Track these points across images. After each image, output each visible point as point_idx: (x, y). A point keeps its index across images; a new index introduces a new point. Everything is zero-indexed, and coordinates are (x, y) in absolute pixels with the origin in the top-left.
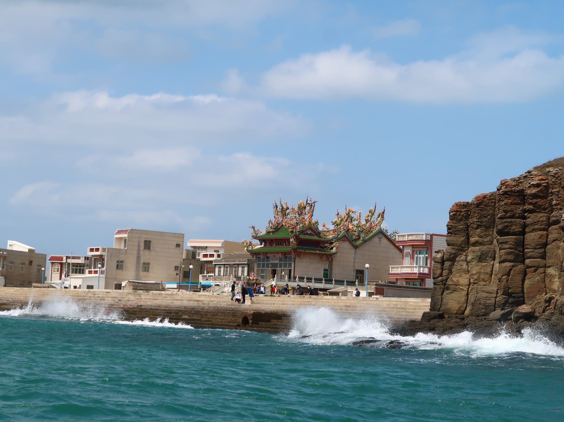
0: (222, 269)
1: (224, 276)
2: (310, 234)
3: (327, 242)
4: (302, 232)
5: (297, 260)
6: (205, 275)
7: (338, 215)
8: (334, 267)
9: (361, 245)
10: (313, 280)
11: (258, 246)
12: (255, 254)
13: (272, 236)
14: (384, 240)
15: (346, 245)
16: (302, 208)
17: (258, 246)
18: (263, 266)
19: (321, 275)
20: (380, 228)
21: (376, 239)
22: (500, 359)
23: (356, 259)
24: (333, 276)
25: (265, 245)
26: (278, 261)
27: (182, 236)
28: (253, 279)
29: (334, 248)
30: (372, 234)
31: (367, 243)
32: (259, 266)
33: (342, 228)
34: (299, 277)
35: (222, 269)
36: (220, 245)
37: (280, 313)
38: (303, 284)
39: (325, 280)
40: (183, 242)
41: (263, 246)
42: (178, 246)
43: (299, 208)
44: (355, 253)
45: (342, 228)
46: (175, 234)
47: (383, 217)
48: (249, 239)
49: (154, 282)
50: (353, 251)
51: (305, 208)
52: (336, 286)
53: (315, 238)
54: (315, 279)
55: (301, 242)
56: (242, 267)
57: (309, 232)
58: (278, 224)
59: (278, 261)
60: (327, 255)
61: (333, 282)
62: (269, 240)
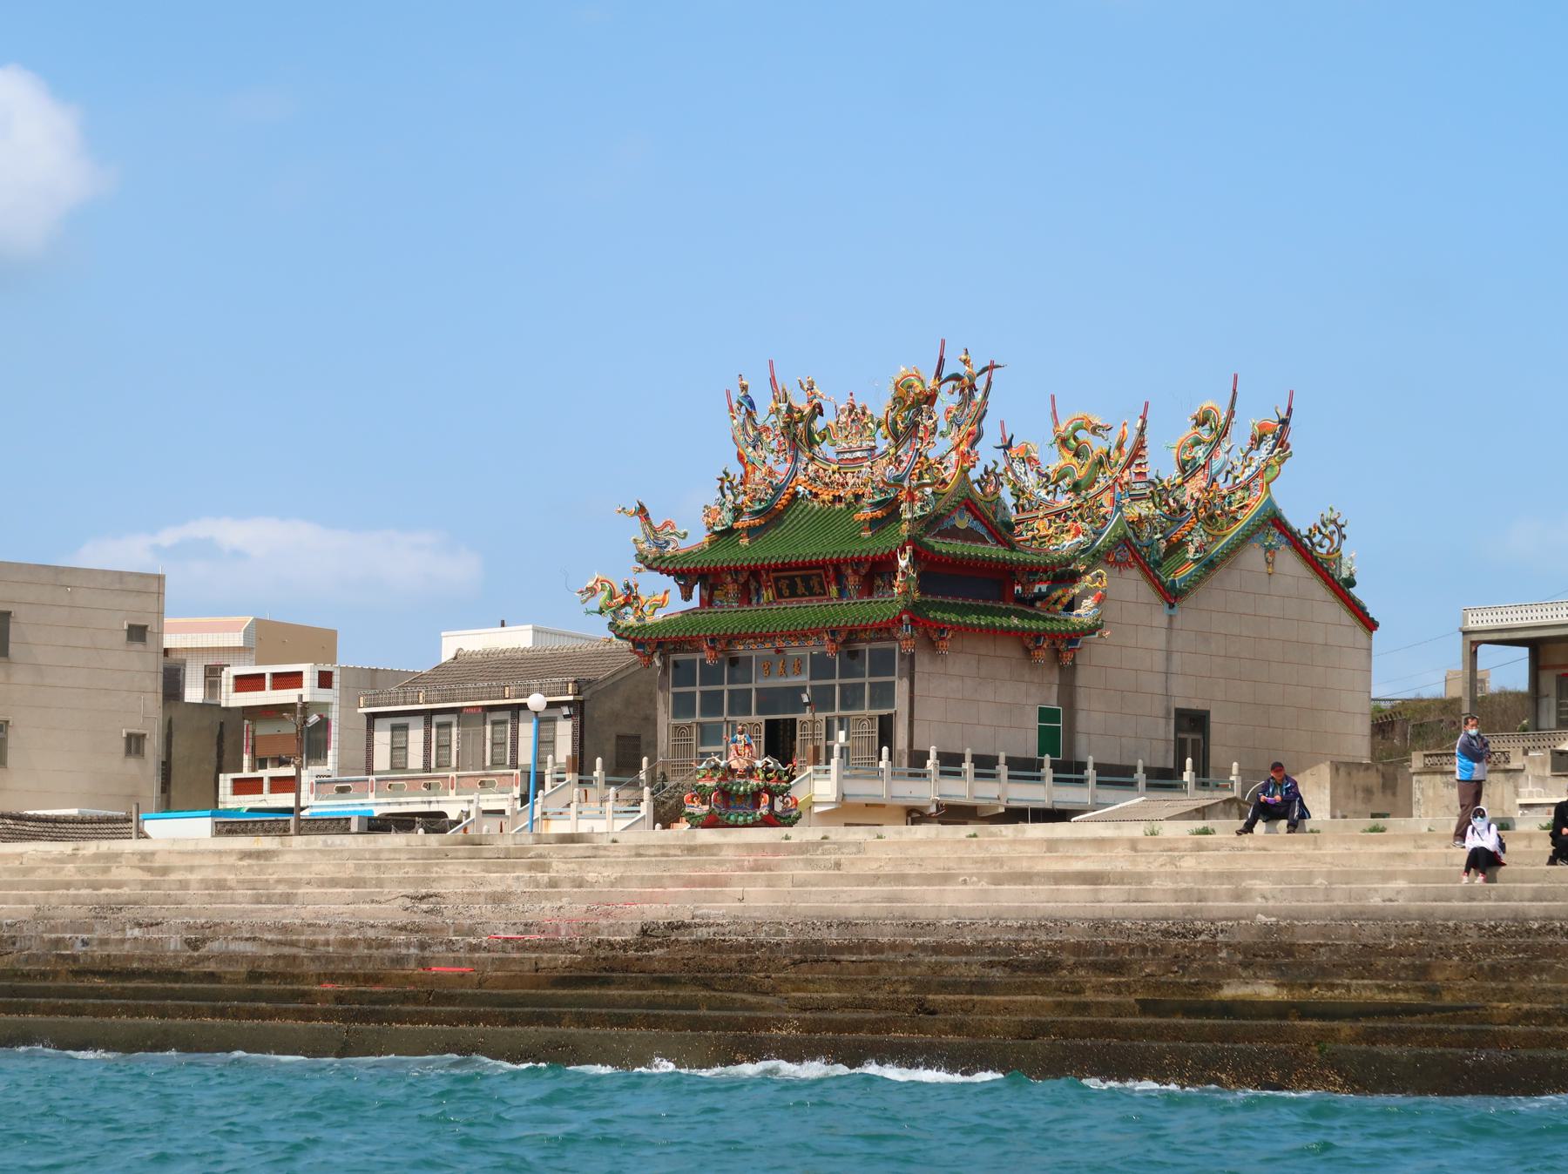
0: (416, 736)
1: (427, 768)
2: (969, 535)
3: (1033, 571)
4: (931, 523)
5: (923, 663)
6: (246, 773)
7: (1007, 446)
8: (1082, 702)
9: (1196, 581)
10: (1002, 769)
11: (666, 601)
12: (660, 644)
13: (746, 551)
14: (1288, 561)
15: (1132, 586)
16: (913, 406)
17: (666, 601)
18: (712, 704)
19: (1028, 745)
20: (1270, 502)
21: (1253, 556)
23: (1176, 657)
24: (1082, 743)
25: (707, 602)
26: (803, 679)
27: (151, 586)
28: (750, 772)
29: (1088, 603)
30: (1236, 529)
31: (1221, 572)
32: (683, 706)
33: (1106, 499)
34: (939, 755)
35: (416, 736)
36: (237, 640)
37: (832, 937)
38: (961, 790)
39: (1055, 767)
41: (695, 602)
42: (137, 633)
43: (898, 400)
44: (1170, 627)
45: (1106, 499)
46: (121, 575)
47: (1281, 442)
48: (624, 571)
49: (73, 812)
50: (1161, 615)
51: (931, 398)
52: (1106, 794)
53: (992, 550)
54: (1012, 763)
55: (937, 573)
56: (394, 728)
57: (963, 521)
58: (778, 490)
59: (803, 679)
60: (1054, 636)
61: (1090, 772)
62: (737, 570)
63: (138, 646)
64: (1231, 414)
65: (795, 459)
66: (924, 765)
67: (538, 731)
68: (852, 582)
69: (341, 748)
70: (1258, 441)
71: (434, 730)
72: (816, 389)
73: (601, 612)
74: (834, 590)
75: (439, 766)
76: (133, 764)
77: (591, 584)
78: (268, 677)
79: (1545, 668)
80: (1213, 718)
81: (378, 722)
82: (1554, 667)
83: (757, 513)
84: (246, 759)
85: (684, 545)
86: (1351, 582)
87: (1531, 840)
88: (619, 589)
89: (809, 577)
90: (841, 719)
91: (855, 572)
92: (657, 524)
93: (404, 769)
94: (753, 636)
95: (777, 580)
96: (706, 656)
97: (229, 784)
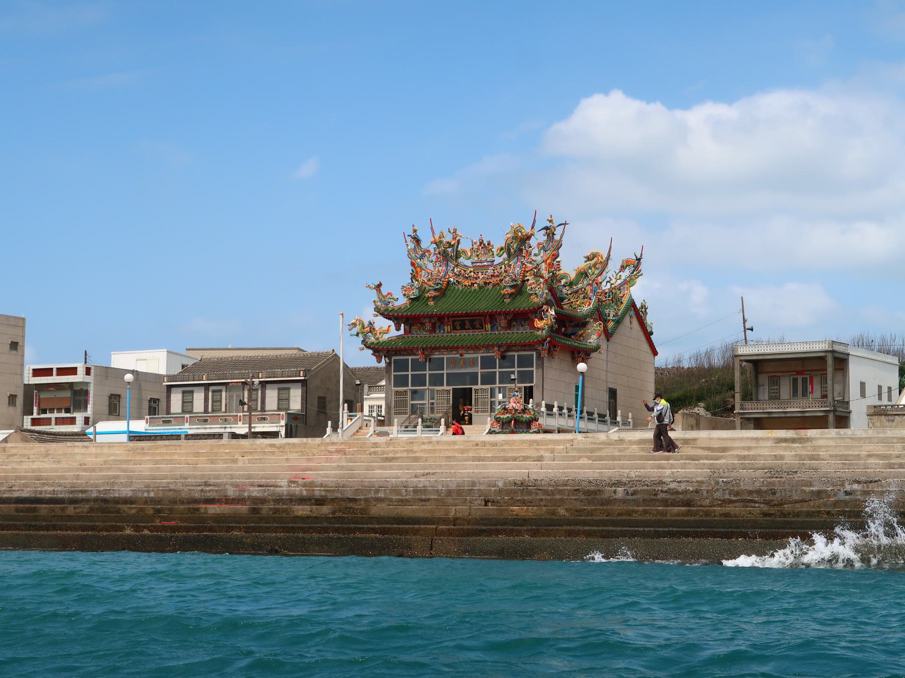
0: (199, 398)
1: (206, 411)
6: (35, 416)
11: (387, 330)
13: (432, 307)
16: (519, 243)
17: (387, 330)
18: (419, 380)
22: (353, 553)
40: (23, 336)
41: (402, 332)
45: (589, 288)
46: (8, 317)
48: (368, 314)
51: (529, 237)
63: (14, 352)
64: (609, 255)
65: (447, 265)
66: (552, 410)
67: (279, 394)
68: (503, 323)
69: (94, 404)
70: (623, 268)
71: (210, 394)
72: (458, 232)
73: (357, 335)
74: (488, 327)
75: (213, 411)
76: (11, 409)
77: (354, 321)
78: (55, 370)
79: (762, 373)
80: (618, 392)
81: (173, 390)
82: (768, 372)
83: (436, 290)
84: (35, 409)
85: (397, 304)
86: (652, 333)
87: (246, 462)
88: (366, 324)
89: (474, 320)
90: (499, 388)
91: (505, 318)
92: (385, 293)
93: (191, 412)
94: (444, 348)
95: (453, 321)
96: (419, 357)
97: (29, 421)
